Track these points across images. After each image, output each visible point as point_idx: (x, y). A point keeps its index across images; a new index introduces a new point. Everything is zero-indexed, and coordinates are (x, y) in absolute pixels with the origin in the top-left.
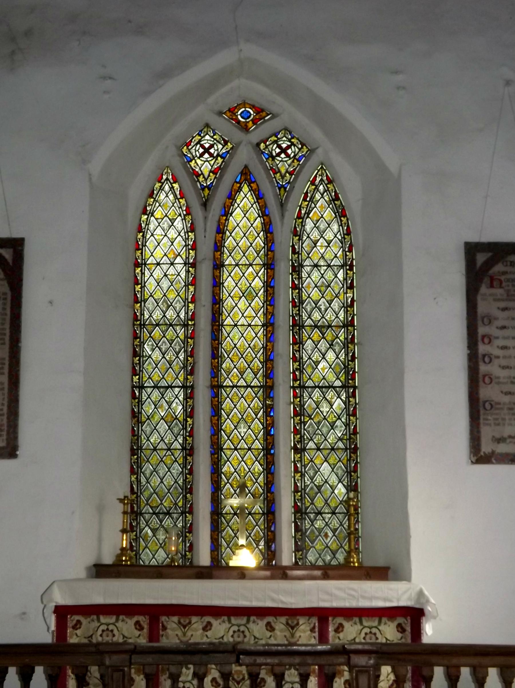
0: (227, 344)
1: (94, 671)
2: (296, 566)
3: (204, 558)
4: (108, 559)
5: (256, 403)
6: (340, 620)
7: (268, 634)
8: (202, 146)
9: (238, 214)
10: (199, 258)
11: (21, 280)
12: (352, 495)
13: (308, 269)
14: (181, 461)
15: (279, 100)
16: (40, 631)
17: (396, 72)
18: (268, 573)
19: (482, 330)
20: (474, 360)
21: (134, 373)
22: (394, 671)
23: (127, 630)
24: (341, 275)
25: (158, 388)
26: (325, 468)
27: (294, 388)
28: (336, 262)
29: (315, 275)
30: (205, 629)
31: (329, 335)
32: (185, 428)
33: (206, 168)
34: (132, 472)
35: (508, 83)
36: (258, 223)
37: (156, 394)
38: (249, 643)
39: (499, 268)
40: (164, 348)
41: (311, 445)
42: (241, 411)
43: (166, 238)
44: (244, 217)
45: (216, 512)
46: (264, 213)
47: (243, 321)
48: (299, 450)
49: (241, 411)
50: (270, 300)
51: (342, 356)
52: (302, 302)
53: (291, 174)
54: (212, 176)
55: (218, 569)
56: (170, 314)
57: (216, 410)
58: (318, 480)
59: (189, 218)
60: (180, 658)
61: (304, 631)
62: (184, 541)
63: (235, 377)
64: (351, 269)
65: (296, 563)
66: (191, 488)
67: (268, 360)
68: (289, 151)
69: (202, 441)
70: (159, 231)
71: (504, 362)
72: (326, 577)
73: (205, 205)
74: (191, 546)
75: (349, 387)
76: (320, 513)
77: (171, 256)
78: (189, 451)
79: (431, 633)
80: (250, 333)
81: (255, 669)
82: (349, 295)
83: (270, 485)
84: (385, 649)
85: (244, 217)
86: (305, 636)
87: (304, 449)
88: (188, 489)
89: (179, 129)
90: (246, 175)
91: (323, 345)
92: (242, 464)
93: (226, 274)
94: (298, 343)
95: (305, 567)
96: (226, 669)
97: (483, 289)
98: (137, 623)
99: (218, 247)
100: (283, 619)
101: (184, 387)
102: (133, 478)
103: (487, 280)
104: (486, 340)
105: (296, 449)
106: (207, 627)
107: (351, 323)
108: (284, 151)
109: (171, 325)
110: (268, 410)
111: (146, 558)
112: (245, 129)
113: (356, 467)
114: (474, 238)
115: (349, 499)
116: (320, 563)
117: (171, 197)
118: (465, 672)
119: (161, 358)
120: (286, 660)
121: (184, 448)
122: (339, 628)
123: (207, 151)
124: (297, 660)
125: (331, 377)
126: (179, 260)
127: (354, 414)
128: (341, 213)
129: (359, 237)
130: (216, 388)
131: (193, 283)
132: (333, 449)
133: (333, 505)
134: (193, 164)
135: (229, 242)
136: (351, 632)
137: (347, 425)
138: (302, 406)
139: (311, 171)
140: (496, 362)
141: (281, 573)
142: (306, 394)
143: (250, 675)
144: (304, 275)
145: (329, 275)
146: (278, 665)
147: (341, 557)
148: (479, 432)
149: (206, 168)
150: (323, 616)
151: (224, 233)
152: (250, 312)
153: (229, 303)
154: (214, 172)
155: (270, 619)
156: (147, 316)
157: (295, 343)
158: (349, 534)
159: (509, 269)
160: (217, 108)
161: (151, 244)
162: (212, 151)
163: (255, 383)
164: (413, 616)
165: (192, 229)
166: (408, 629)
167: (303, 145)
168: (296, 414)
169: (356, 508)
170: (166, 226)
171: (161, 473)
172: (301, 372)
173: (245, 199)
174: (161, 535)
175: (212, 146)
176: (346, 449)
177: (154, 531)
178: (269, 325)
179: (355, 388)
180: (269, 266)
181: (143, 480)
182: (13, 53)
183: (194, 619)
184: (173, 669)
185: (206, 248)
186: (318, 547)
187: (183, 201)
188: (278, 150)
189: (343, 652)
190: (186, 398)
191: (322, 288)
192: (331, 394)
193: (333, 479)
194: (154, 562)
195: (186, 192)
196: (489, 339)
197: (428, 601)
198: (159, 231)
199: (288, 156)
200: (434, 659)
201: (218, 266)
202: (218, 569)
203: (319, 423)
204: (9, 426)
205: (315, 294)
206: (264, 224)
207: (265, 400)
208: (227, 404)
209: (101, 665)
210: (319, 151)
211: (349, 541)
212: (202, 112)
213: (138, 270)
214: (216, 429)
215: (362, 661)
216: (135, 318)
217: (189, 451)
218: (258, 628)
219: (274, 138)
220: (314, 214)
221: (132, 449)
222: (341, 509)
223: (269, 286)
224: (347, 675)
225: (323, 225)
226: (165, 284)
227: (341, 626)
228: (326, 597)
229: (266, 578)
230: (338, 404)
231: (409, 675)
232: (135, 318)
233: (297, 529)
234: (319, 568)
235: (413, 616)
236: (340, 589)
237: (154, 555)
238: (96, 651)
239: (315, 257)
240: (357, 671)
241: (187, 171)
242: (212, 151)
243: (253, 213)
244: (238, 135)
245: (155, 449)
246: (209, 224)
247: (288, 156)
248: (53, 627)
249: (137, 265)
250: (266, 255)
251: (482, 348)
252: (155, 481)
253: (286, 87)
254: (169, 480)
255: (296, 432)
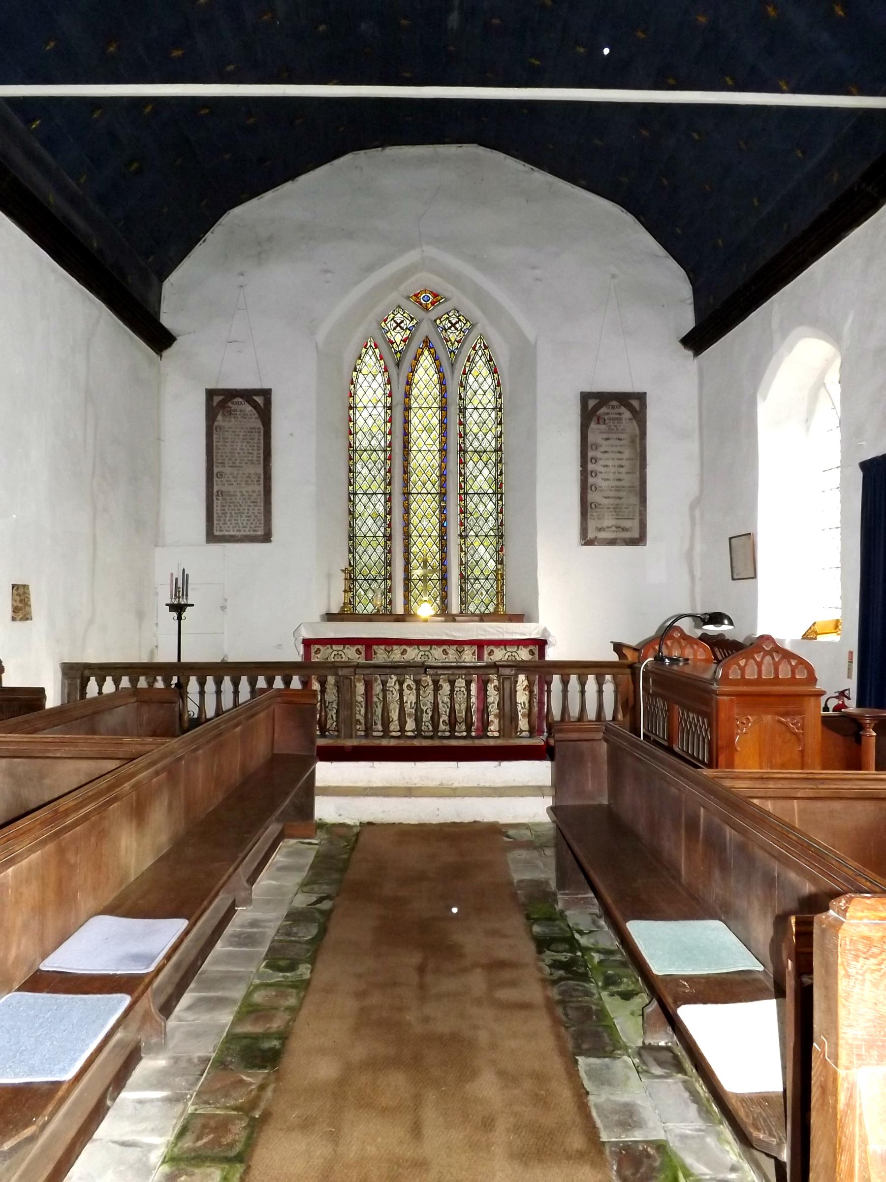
0: (413, 464)
1: (331, 680)
2: (461, 614)
3: (400, 610)
4: (335, 610)
5: (435, 505)
6: (492, 647)
7: (445, 656)
8: (395, 322)
9: (420, 372)
10: (394, 403)
11: (270, 419)
12: (499, 566)
13: (470, 411)
14: (383, 544)
15: (451, 288)
16: (295, 654)
17: (533, 268)
18: (443, 619)
19: (590, 454)
20: (585, 474)
21: (350, 484)
22: (527, 678)
23: (351, 654)
24: (493, 415)
25: (366, 494)
26: (482, 550)
27: (460, 494)
28: (490, 406)
29: (475, 415)
30: (402, 654)
31: (485, 457)
32: (385, 522)
33: (398, 338)
34: (350, 552)
35: (614, 276)
36: (435, 378)
37: (365, 499)
38: (431, 662)
39: (603, 410)
40: (370, 467)
41: (472, 533)
42: (424, 512)
43: (371, 389)
44: (425, 375)
45: (407, 579)
46: (439, 370)
47: (425, 448)
48: (463, 537)
49: (424, 512)
50: (444, 433)
51: (493, 472)
52: (466, 434)
53: (458, 342)
54: (403, 343)
55: (407, 616)
56: (374, 443)
57: (407, 510)
58: (476, 557)
59: (386, 374)
60: (388, 671)
61: (468, 655)
62: (386, 598)
63: (419, 487)
64: (500, 411)
65: (462, 612)
66: (390, 562)
67: (443, 475)
68: (457, 325)
69: (397, 531)
70: (365, 384)
71: (605, 476)
72: (482, 620)
73: (398, 365)
74: (390, 601)
75: (498, 493)
76: (477, 579)
77: (374, 402)
78: (388, 538)
79: (552, 654)
80: (429, 457)
81: (437, 678)
82: (499, 429)
83: (443, 561)
84: (521, 664)
85: (425, 375)
86: (469, 656)
87: (467, 536)
88: (388, 564)
89: (379, 309)
90: (427, 343)
91: (480, 465)
92: (425, 546)
93: (413, 414)
94: (463, 462)
95: (467, 615)
96: (418, 677)
97: (593, 425)
98: (357, 650)
99: (408, 395)
100: (454, 647)
101: (384, 494)
102: (351, 556)
103: (595, 419)
104: (593, 461)
105: (461, 536)
106: (404, 652)
107: (500, 449)
108: (453, 325)
109: (375, 451)
110: (443, 509)
111: (360, 609)
112: (426, 309)
113: (502, 548)
114: (587, 389)
115: (498, 569)
116: (477, 612)
117: (373, 357)
118: (574, 678)
119: (369, 475)
120: (457, 671)
121: (384, 536)
122: (491, 653)
123: (398, 325)
124: (464, 671)
125: (486, 487)
126: (380, 404)
127: (501, 512)
128: (494, 371)
129: (506, 387)
130: (407, 494)
131: (390, 421)
132: (486, 536)
133: (486, 574)
134: (389, 334)
135: (415, 392)
136: (499, 655)
137: (496, 519)
138: (466, 507)
139: (472, 340)
140: (600, 476)
141: (453, 618)
142: (468, 498)
143: (433, 681)
144: (468, 415)
145: (485, 415)
146: (452, 674)
147: (491, 608)
148: (587, 524)
149: (398, 338)
150: (480, 645)
151: (411, 385)
152: (430, 442)
153: (414, 435)
154: (404, 341)
155: (445, 647)
156: (358, 444)
157: (461, 463)
158: (497, 593)
159: (610, 411)
160: (406, 294)
161: (360, 393)
162: (402, 325)
163: (434, 491)
164: (541, 644)
165: (389, 382)
166: (537, 652)
167: (467, 321)
168: (461, 512)
169: (502, 576)
170: (370, 380)
171: (370, 553)
172: (465, 483)
173: (426, 360)
174: (370, 594)
175: (402, 322)
176: (495, 536)
177: (365, 591)
178: (443, 450)
179: (502, 494)
180: (443, 408)
181: (357, 558)
182: (260, 253)
183: (395, 647)
184: (383, 678)
185: (399, 396)
186: (476, 602)
187: (382, 362)
188: (449, 325)
189: (495, 666)
190: (386, 502)
191: (480, 426)
192: (485, 499)
193: (487, 557)
194: (365, 612)
195: (384, 356)
196: (595, 460)
197: (550, 635)
198: (365, 384)
199: (456, 329)
200: (553, 670)
201: (408, 408)
202: (407, 616)
203: (478, 518)
204: (265, 521)
205: (475, 429)
206: (439, 378)
207: (440, 502)
208: (414, 506)
209: (336, 674)
210: (479, 325)
211: (498, 598)
212: (394, 297)
213: (351, 412)
214: (407, 524)
215: (507, 671)
216: (350, 446)
217: (388, 538)
218: (437, 653)
219: (446, 316)
220: (475, 372)
221: (350, 536)
222: (492, 576)
223: (443, 423)
224: (496, 683)
225: (481, 379)
226: (370, 421)
227: (492, 651)
228: (482, 633)
229: (442, 621)
230: (491, 506)
231: (537, 682)
232: (350, 446)
233: (462, 590)
234: (477, 615)
235: (541, 644)
236: (494, 628)
237: (365, 607)
238: (334, 667)
239: (475, 402)
240: (502, 679)
241: (385, 340)
242: (402, 325)
243: (432, 371)
244: (421, 313)
245: (365, 536)
246: (401, 379)
247: (456, 329)
248: (302, 652)
249: (351, 408)
250: (441, 401)
251: (590, 467)
252: (365, 557)
253: (456, 279)
254: (375, 557)
255: (461, 524)
